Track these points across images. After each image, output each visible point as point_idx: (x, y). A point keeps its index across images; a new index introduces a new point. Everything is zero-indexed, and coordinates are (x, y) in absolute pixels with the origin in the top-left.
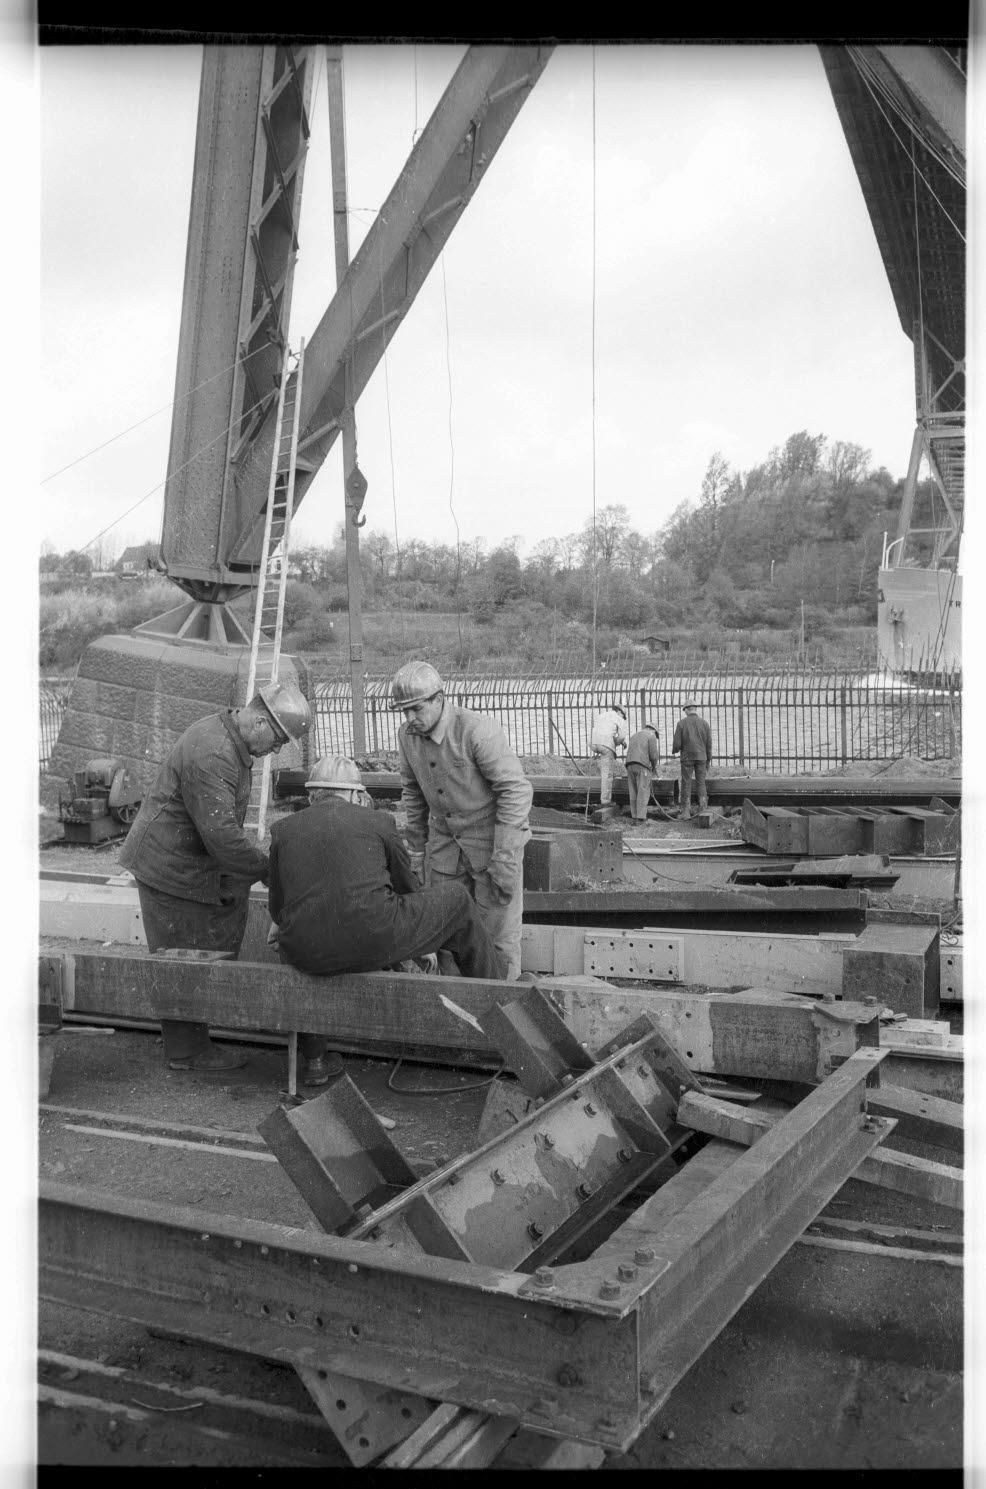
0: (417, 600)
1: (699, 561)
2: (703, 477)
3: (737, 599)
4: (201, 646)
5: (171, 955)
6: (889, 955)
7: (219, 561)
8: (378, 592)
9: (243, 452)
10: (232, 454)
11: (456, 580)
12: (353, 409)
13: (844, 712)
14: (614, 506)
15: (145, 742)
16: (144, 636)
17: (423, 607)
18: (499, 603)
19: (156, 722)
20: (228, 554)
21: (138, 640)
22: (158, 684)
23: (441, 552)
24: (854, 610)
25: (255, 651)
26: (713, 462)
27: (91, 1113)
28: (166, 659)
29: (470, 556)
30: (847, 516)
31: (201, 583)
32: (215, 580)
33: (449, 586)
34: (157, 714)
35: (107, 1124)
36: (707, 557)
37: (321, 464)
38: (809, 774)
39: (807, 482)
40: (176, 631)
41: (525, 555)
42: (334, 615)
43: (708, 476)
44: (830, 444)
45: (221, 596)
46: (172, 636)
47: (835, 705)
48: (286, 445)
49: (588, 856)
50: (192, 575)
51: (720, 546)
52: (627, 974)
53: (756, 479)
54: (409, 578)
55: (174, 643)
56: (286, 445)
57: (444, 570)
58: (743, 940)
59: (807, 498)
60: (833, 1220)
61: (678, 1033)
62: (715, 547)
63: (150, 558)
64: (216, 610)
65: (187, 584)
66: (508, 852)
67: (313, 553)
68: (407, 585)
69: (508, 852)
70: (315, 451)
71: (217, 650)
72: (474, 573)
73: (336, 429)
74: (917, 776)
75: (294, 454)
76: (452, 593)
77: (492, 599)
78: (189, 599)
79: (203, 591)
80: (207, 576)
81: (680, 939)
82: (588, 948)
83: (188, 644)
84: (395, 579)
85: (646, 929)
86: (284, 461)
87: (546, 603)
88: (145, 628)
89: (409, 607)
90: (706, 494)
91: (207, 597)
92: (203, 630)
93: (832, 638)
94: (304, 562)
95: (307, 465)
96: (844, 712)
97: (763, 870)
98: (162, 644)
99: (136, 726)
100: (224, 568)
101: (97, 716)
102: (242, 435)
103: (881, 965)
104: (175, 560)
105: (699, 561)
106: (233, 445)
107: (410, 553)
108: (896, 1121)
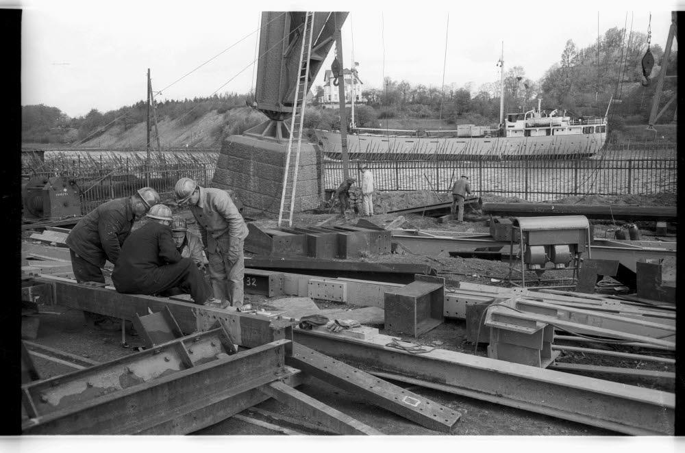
0: (421, 113)
1: (559, 93)
2: (562, 52)
3: (577, 111)
4: (271, 140)
5: (84, 285)
6: (402, 296)
7: (279, 102)
8: (403, 109)
9: (289, 53)
10: (285, 54)
11: (439, 104)
12: (340, 31)
13: (576, 171)
14: (517, 66)
15: (247, 181)
16: (248, 135)
17: (423, 116)
18: (459, 114)
19: (251, 173)
20: (283, 99)
21: (246, 137)
22: (252, 157)
23: (433, 91)
24: (637, 116)
25: (291, 142)
26: (568, 44)
27: (44, 347)
28: (256, 146)
29: (448, 92)
30: (636, 69)
31: (272, 112)
32: (277, 110)
33: (436, 107)
34: (252, 170)
35: (52, 354)
36: (563, 91)
37: (326, 57)
38: (547, 202)
39: (616, 53)
40: (261, 133)
41: (474, 93)
42: (381, 120)
43: (565, 51)
44: (628, 32)
45: (281, 118)
46: (259, 135)
47: (572, 168)
48: (306, 48)
49: (373, 242)
50: (268, 108)
51: (570, 85)
52: (323, 298)
53: (590, 51)
54: (418, 103)
55: (260, 138)
56: (306, 48)
57: (434, 99)
58: (370, 286)
59: (616, 61)
60: (570, 416)
61: (231, 328)
62: (568, 86)
63: (248, 102)
64: (279, 125)
65: (266, 112)
66: (233, 247)
67: (373, 91)
68: (416, 106)
69: (233, 247)
70: (323, 51)
71: (278, 142)
72: (450, 100)
73: (332, 41)
74: (598, 205)
75: (309, 53)
76: (438, 110)
77: (456, 112)
78: (268, 119)
79: (274, 116)
80: (274, 109)
81: (345, 284)
82: (310, 285)
83: (266, 139)
84: (412, 103)
85: (339, 278)
86: (305, 58)
87: (482, 114)
88: (251, 132)
89: (417, 117)
90: (563, 61)
91: (275, 118)
92: (273, 133)
93: (624, 131)
94: (369, 97)
95: (317, 57)
96: (576, 171)
97: (490, 249)
98: (255, 139)
99: (243, 175)
100: (281, 104)
101: (228, 171)
102: (290, 43)
103: (399, 301)
104: (261, 102)
105: (559, 93)
106: (285, 49)
107: (418, 91)
108: (298, 371)
